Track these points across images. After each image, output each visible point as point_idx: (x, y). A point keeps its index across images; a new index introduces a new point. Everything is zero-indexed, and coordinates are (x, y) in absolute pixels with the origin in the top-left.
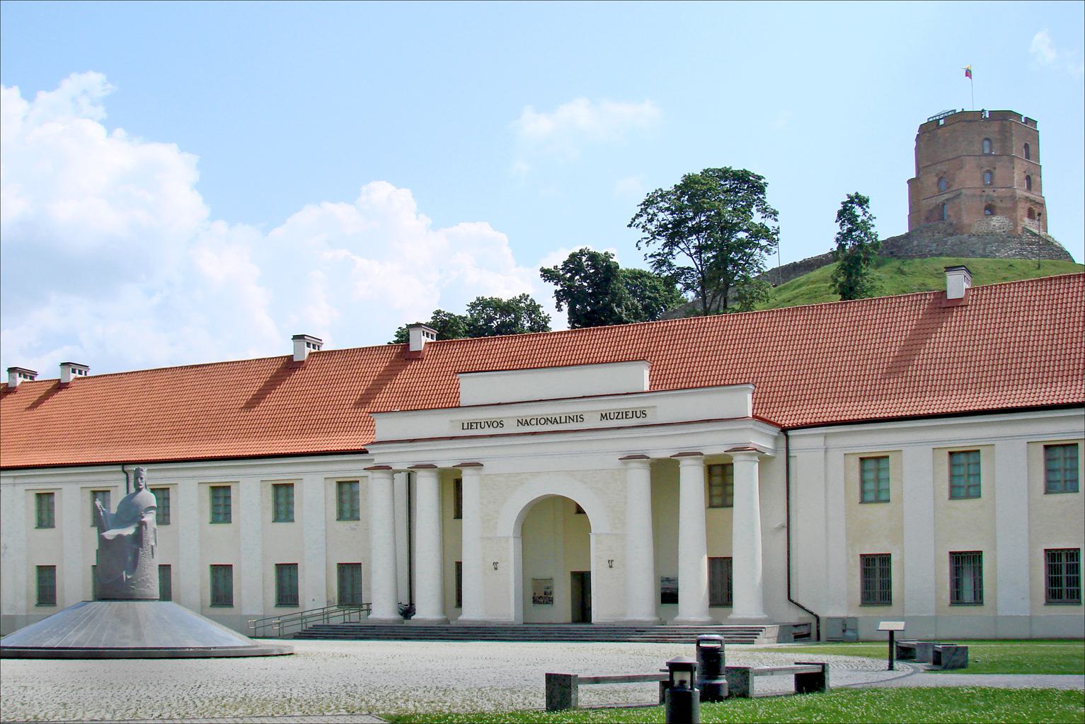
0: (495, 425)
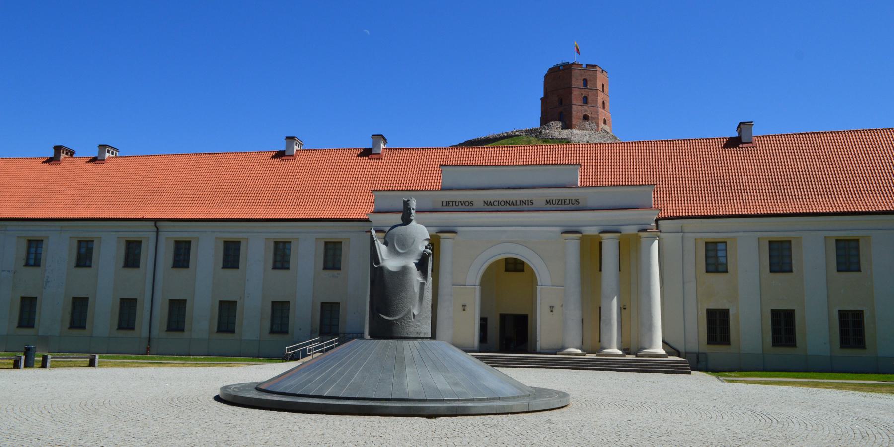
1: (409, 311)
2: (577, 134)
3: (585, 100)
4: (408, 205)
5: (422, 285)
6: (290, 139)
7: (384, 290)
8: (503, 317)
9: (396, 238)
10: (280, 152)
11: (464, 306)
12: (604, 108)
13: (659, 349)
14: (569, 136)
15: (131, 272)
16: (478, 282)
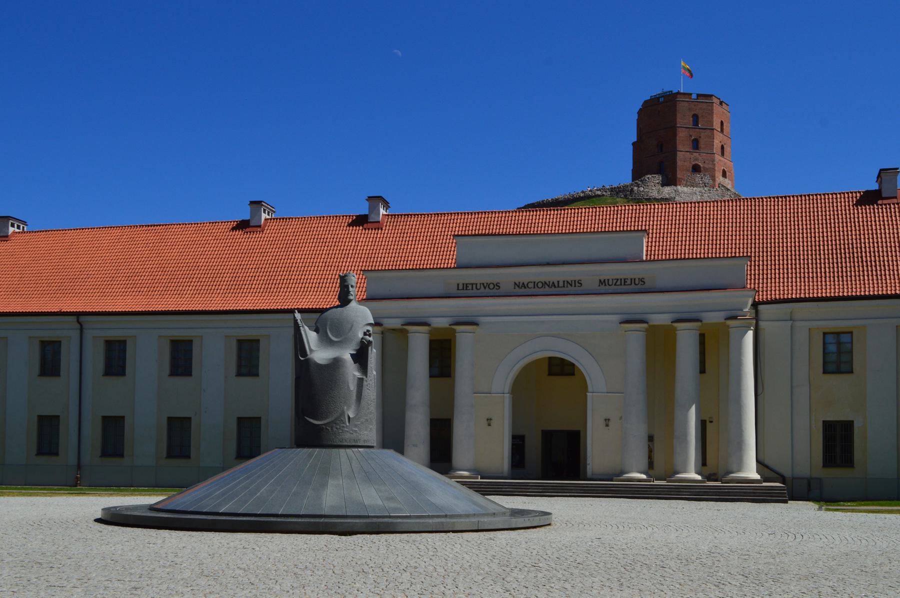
0: (492, 286)
1: (343, 413)
2: (684, 192)
3: (696, 145)
5: (360, 382)
6: (256, 204)
7: (313, 387)
10: (243, 221)
11: (489, 420)
12: (723, 154)
13: (751, 472)
14: (672, 195)
15: (50, 382)
16: (507, 388)
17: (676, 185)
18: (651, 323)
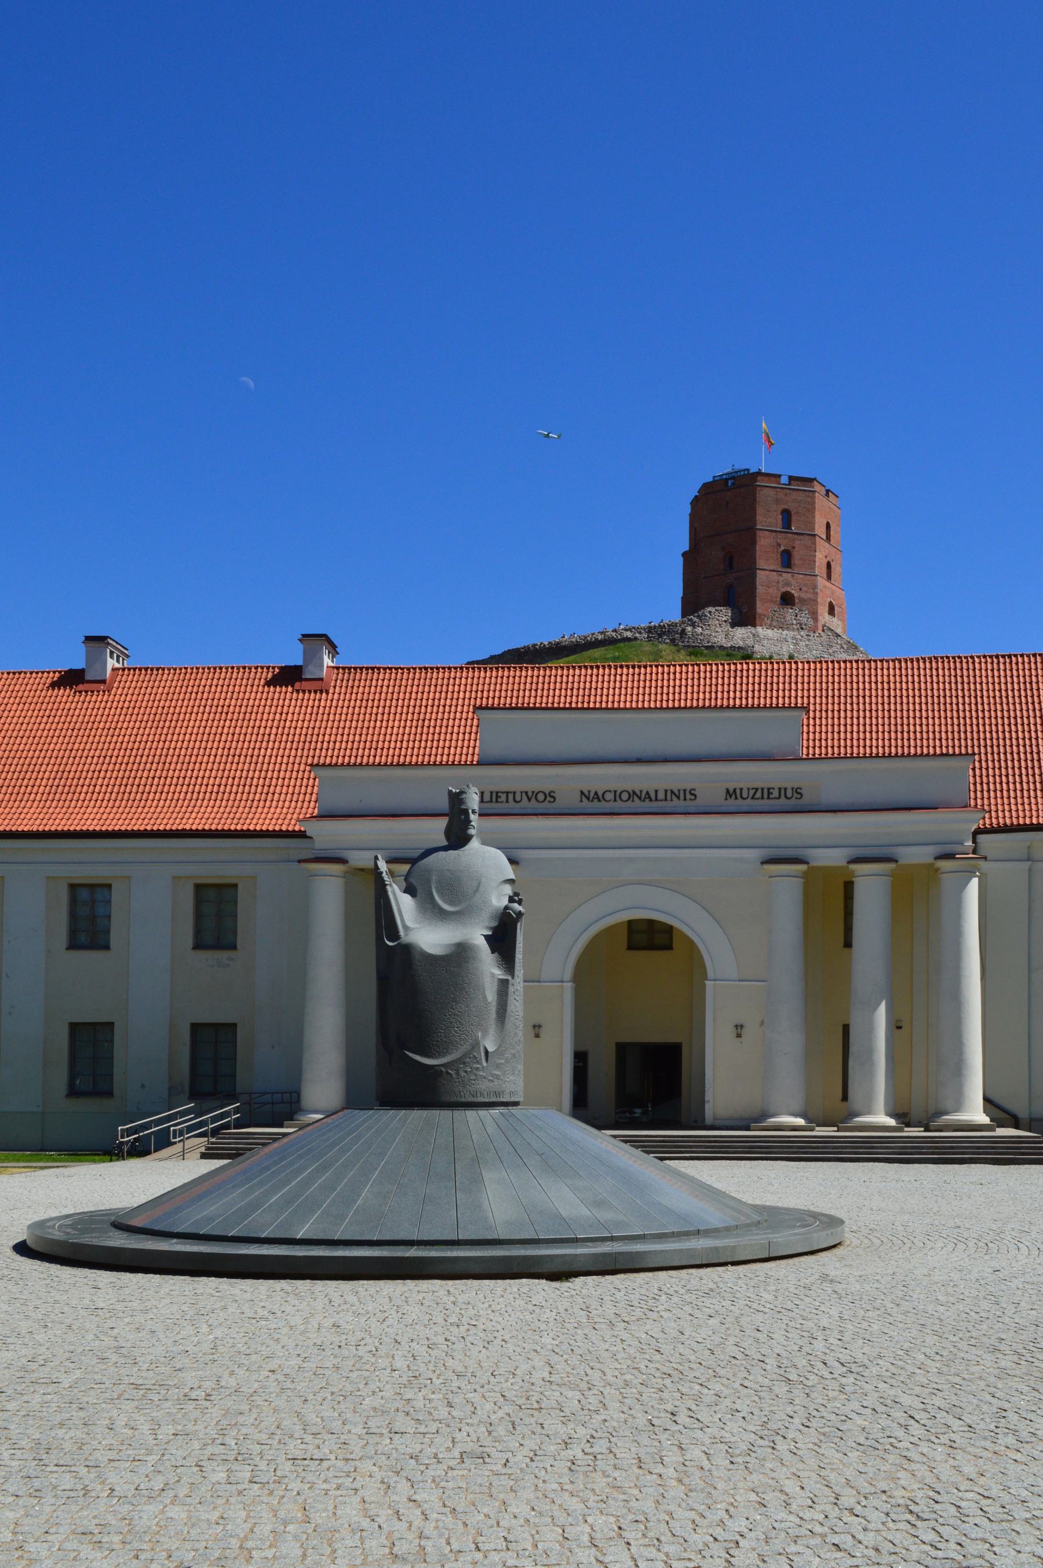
0: (541, 797)
1: (476, 1045)
2: (767, 638)
3: (787, 559)
4: (462, 802)
5: (504, 985)
6: (97, 641)
8: (622, 1049)
9: (434, 878)
12: (829, 577)
14: (750, 642)
16: (568, 974)
17: (754, 625)
18: (813, 864)
